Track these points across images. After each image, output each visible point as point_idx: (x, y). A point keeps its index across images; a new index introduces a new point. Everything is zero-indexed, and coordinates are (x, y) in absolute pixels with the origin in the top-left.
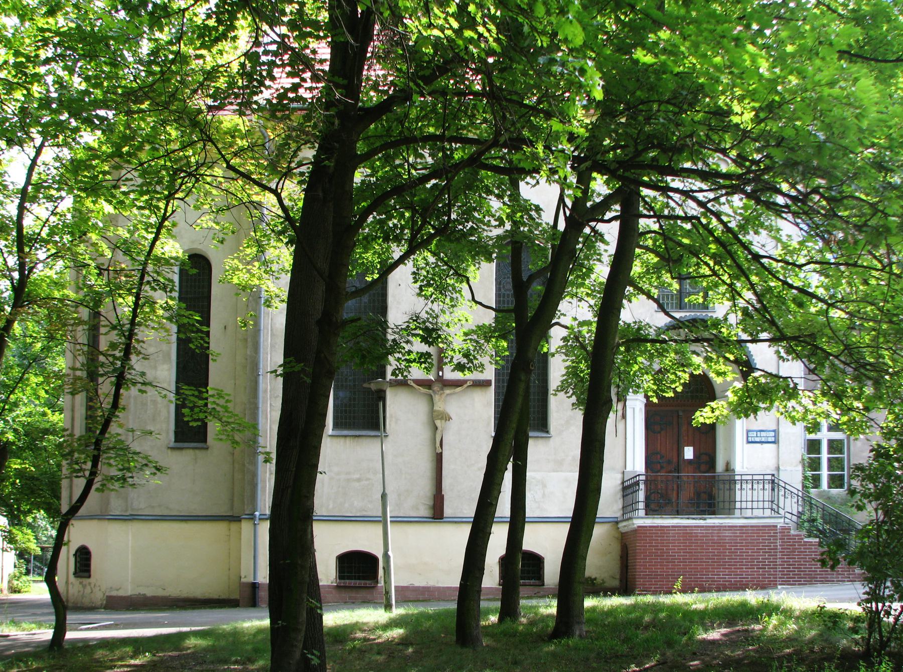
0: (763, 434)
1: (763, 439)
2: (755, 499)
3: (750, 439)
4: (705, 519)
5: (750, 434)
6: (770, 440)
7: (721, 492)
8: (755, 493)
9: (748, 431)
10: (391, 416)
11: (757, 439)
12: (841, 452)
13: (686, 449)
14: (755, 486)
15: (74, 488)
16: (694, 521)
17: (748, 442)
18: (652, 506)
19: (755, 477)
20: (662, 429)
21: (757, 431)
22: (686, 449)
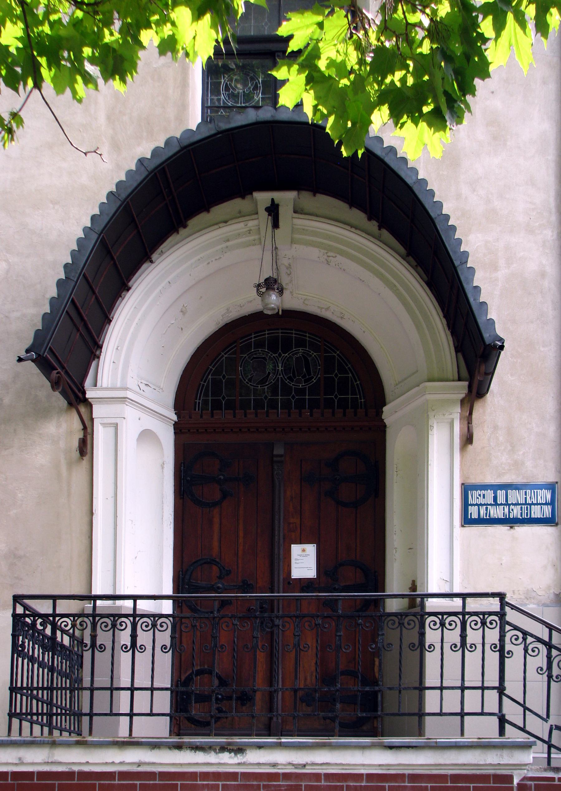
0: (515, 496)
1: (516, 512)
2: (142, 680)
3: (473, 512)
4: (240, 750)
5: (474, 497)
6: (536, 512)
7: (102, 659)
8: (143, 659)
9: (466, 489)
10: (521, 605)
11: (497, 512)
12: (164, 168)
13: (296, 549)
14: (473, 636)
15: (541, 656)
16: (200, 757)
17: (467, 521)
18: (196, 710)
19: (473, 605)
20: (225, 495)
21: (495, 488)
22: (296, 549)
